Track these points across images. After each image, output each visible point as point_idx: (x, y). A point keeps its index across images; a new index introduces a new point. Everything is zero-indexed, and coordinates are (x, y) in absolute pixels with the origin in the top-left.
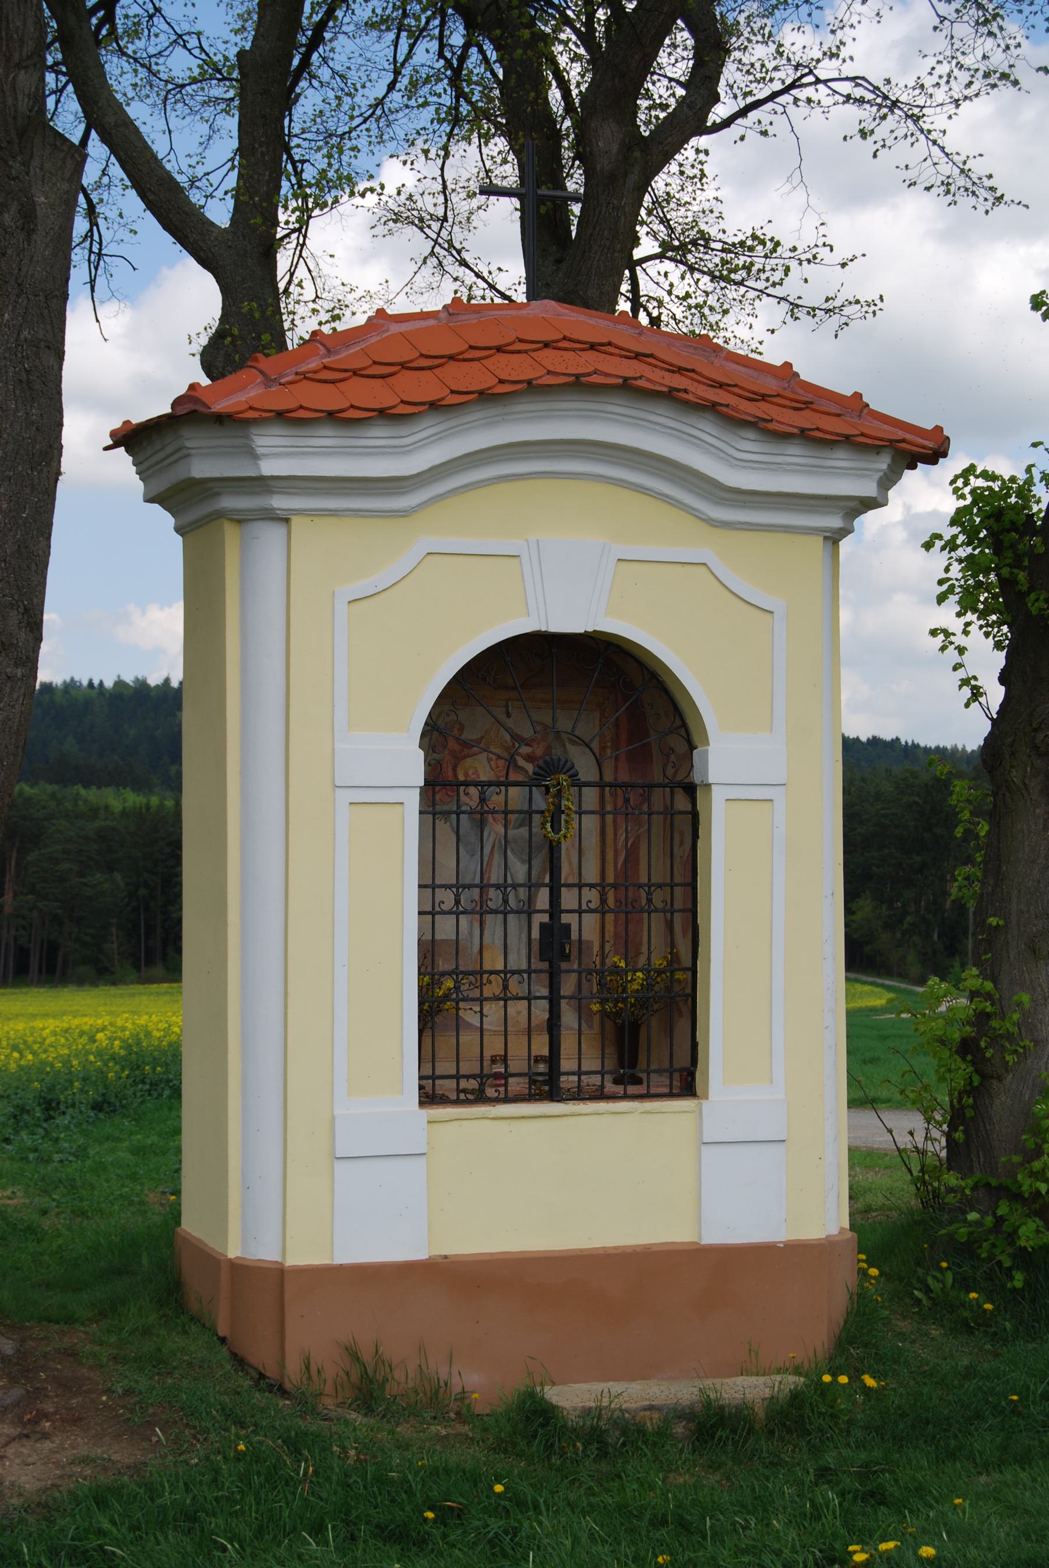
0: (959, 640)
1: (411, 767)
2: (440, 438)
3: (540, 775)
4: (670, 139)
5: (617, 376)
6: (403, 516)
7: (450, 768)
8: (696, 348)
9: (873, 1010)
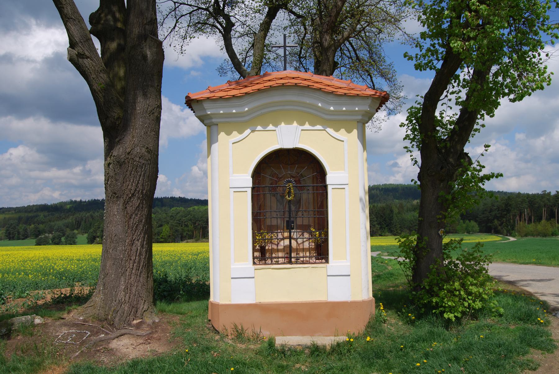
0: (411, 149)
1: (248, 182)
9: (497, 241)
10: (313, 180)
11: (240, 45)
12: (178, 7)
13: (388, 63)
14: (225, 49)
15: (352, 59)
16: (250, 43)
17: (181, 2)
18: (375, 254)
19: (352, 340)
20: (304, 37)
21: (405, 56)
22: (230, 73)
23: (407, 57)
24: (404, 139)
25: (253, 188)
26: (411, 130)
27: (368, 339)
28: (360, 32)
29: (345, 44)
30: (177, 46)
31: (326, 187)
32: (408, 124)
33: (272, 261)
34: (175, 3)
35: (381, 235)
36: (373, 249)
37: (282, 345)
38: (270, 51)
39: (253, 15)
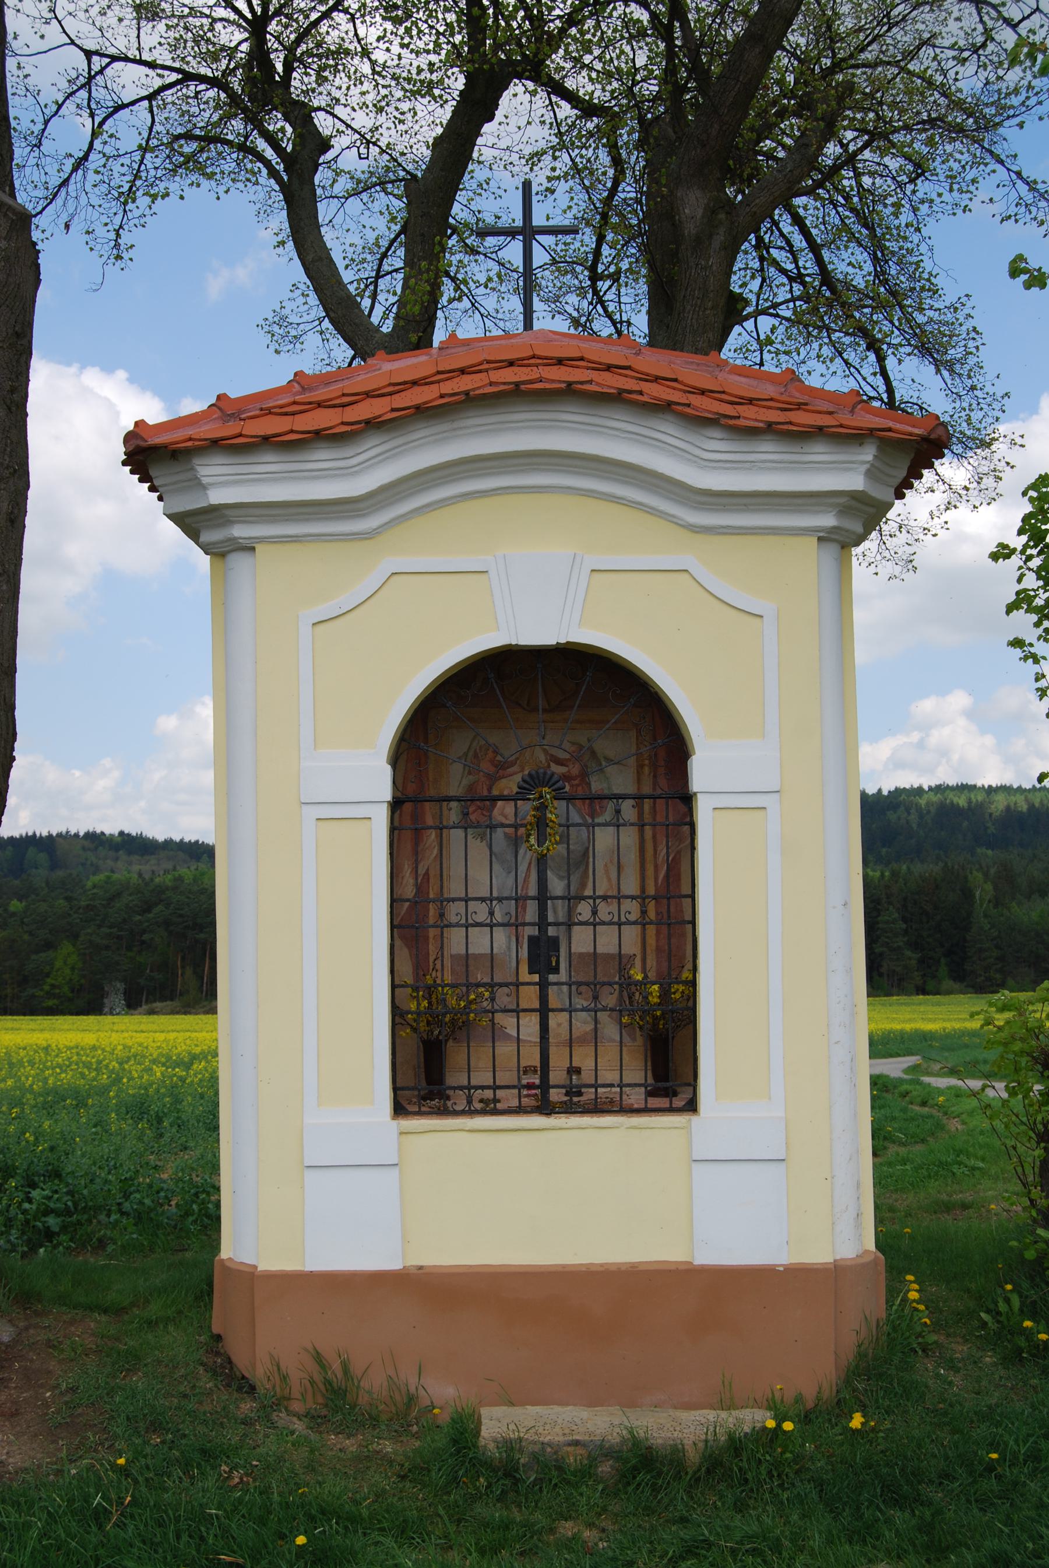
1: (378, 782)
2: (388, 458)
3: (525, 789)
4: (757, 201)
5: (560, 382)
6: (366, 539)
7: (485, 788)
8: (698, 365)
10: (640, 767)
11: (358, 229)
12: (101, 72)
13: (950, 298)
14: (290, 245)
15: (803, 283)
16: (393, 219)
17: (112, 51)
18: (894, 1068)
19: (788, 1426)
20: (613, 191)
21: (1014, 273)
22: (313, 340)
23: (1024, 277)
24: (1010, 608)
25: (396, 805)
26: (1038, 572)
27: (857, 1421)
28: (836, 169)
29: (776, 224)
30: (101, 232)
31: (688, 800)
32: (1026, 546)
33: (470, 1102)
34: (89, 54)
35: (922, 991)
36: (881, 1046)
37: (510, 1446)
38: (473, 251)
39: (405, 106)
